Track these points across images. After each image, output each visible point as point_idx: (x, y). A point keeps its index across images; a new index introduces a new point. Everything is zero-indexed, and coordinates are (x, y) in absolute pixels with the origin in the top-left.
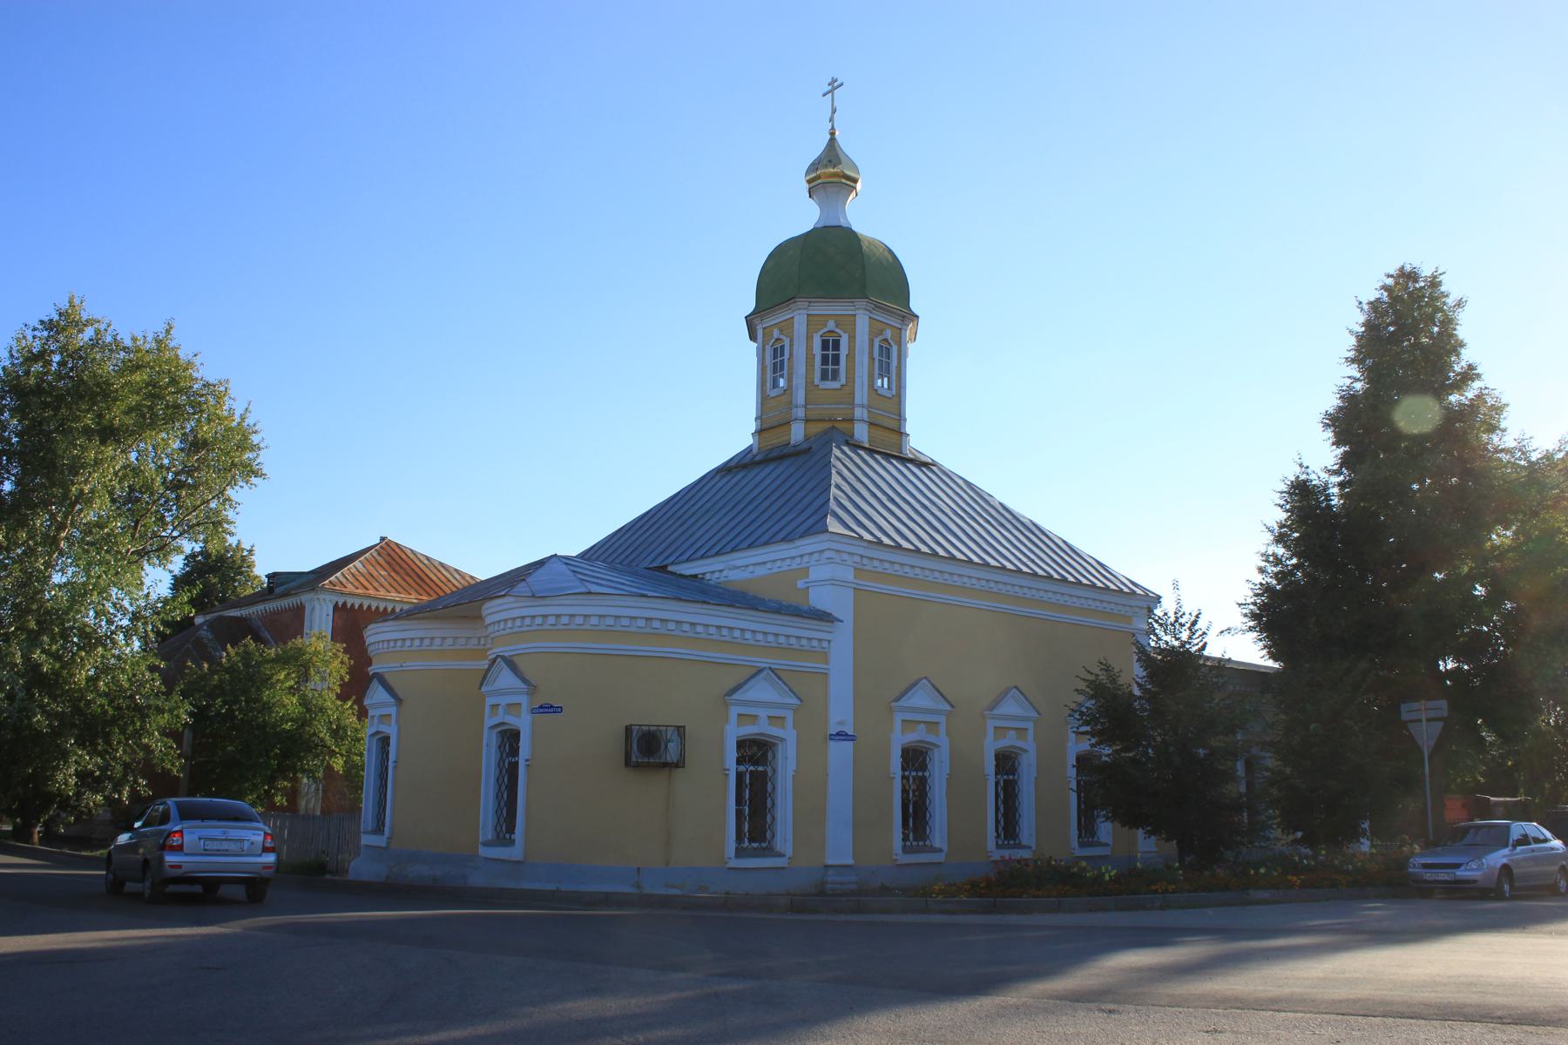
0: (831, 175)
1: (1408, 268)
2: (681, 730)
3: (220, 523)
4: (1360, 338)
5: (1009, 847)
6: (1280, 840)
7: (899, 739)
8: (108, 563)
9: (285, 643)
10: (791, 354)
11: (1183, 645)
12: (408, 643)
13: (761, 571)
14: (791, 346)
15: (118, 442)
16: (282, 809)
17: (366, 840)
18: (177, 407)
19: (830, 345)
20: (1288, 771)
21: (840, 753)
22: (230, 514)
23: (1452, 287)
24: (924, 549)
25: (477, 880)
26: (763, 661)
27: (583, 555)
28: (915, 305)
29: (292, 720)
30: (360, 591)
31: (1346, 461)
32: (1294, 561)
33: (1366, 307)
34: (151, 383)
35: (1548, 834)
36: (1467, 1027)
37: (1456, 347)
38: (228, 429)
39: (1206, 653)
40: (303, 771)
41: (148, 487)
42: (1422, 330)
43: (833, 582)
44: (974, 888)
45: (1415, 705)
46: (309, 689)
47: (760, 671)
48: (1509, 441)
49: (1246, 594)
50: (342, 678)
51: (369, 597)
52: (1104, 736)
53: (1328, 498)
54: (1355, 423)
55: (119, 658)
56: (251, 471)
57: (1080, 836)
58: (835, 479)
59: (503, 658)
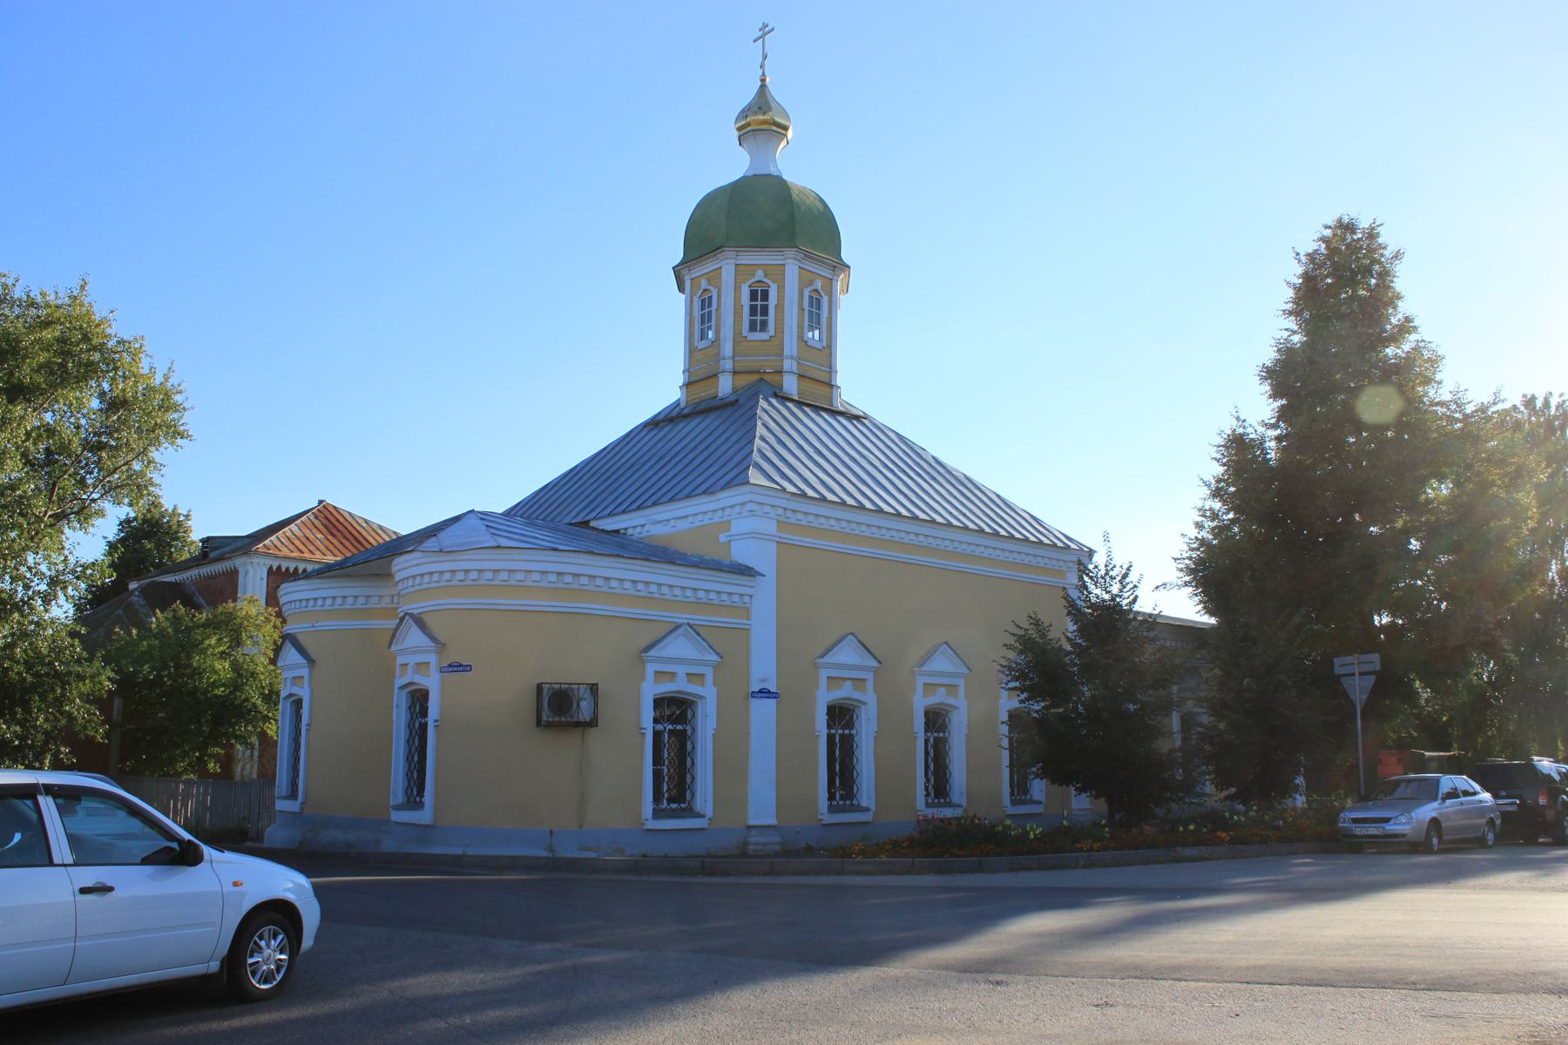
0: (761, 122)
1: (1346, 220)
2: (594, 688)
4: (1297, 289)
5: (939, 805)
6: (1211, 794)
7: (824, 697)
8: (21, 526)
11: (1113, 599)
13: (683, 525)
14: (719, 296)
15: (29, 401)
16: (214, 776)
17: (281, 805)
18: (90, 364)
19: (759, 295)
20: (1222, 726)
21: (763, 714)
23: (1390, 239)
24: (850, 501)
25: (389, 845)
26: (680, 617)
27: (509, 513)
28: (845, 256)
29: (224, 685)
31: (1283, 414)
32: (1231, 516)
33: (1304, 259)
34: (62, 340)
35: (1477, 787)
36: (1378, 994)
38: (149, 388)
39: (1136, 608)
40: (237, 738)
41: (64, 448)
42: (1360, 282)
43: (755, 535)
44: (896, 847)
45: (1349, 659)
46: (238, 654)
47: (678, 627)
48: (1445, 395)
49: (1180, 548)
52: (1033, 692)
53: (1264, 452)
54: (1289, 377)
55: (38, 624)
56: (175, 433)
57: (1012, 794)
58: (760, 430)
59: (411, 615)
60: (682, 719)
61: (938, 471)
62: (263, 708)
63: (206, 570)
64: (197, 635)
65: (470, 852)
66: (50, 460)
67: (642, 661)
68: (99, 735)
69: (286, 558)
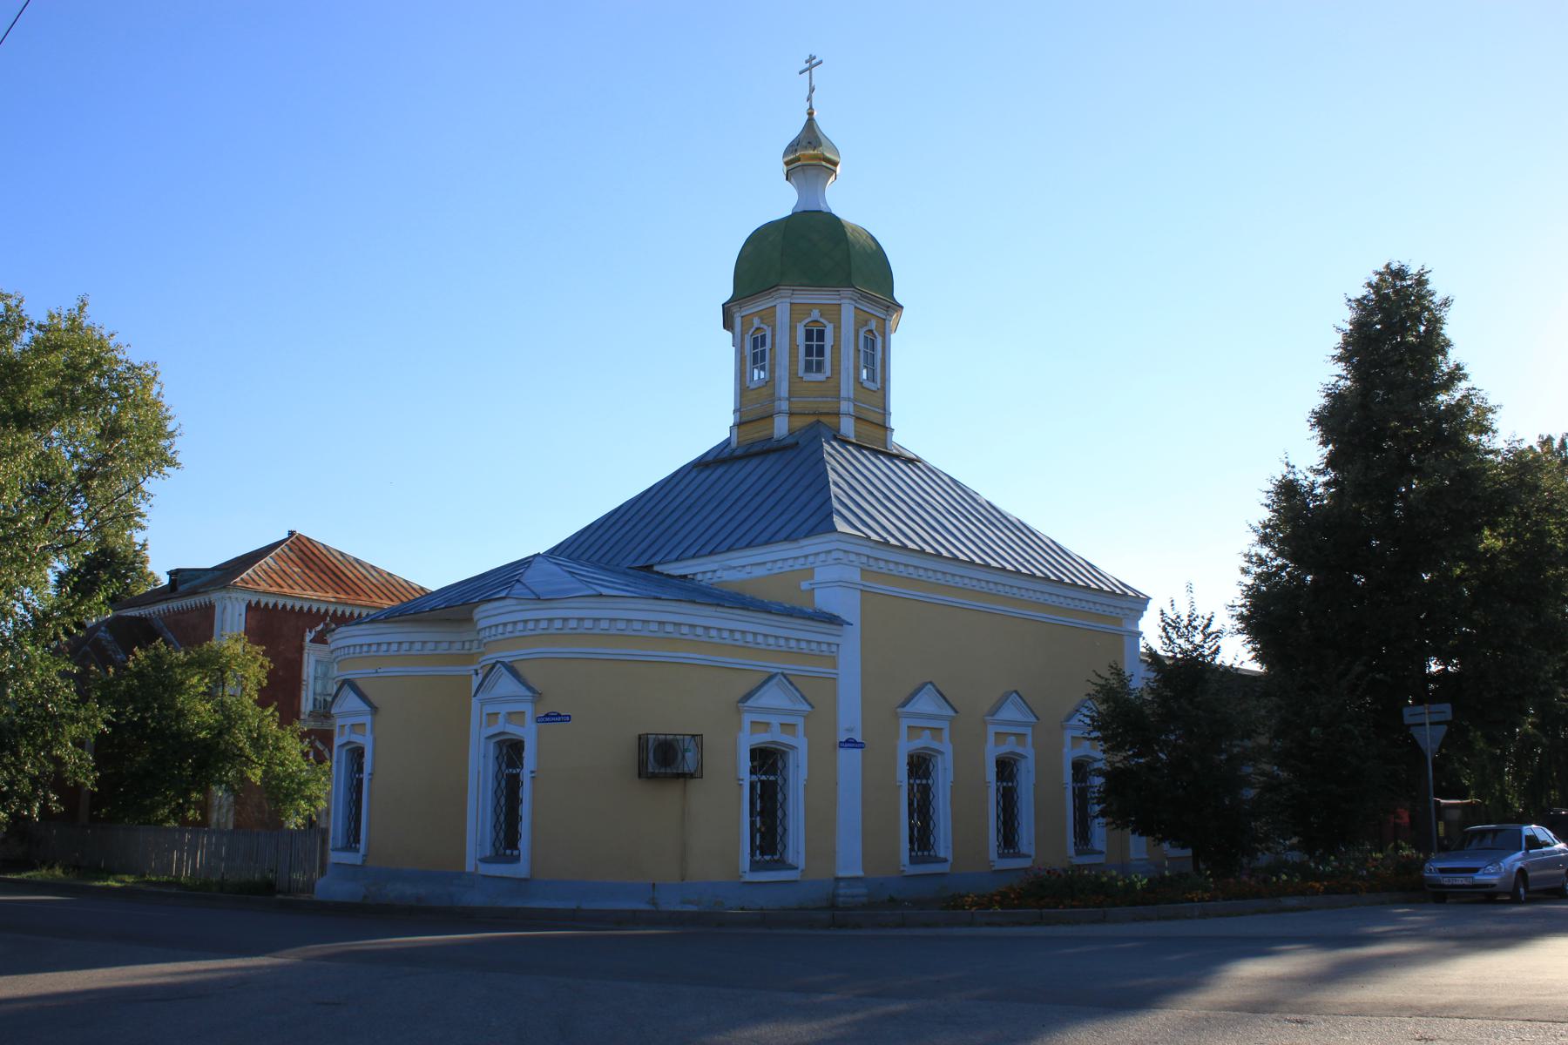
0: (809, 157)
1: (1395, 266)
3: (130, 516)
6: (1289, 850)
7: (905, 747)
9: (201, 645)
10: (773, 344)
12: (384, 647)
13: (759, 572)
14: (773, 336)
16: (195, 823)
19: (815, 335)
22: (143, 508)
23: (1439, 287)
25: (475, 899)
26: (774, 666)
28: (898, 295)
30: (275, 589)
31: (1332, 462)
32: (1279, 562)
34: (72, 365)
37: (1444, 347)
42: (1408, 329)
44: (985, 902)
47: (771, 677)
50: (259, 683)
51: (284, 595)
52: (1113, 742)
58: (832, 476)
59: (503, 663)
60: (773, 769)
61: (994, 517)
62: (248, 750)
63: (175, 605)
64: (178, 674)
65: (585, 906)
66: (44, 491)
67: (739, 712)
68: (89, 781)
69: (265, 593)
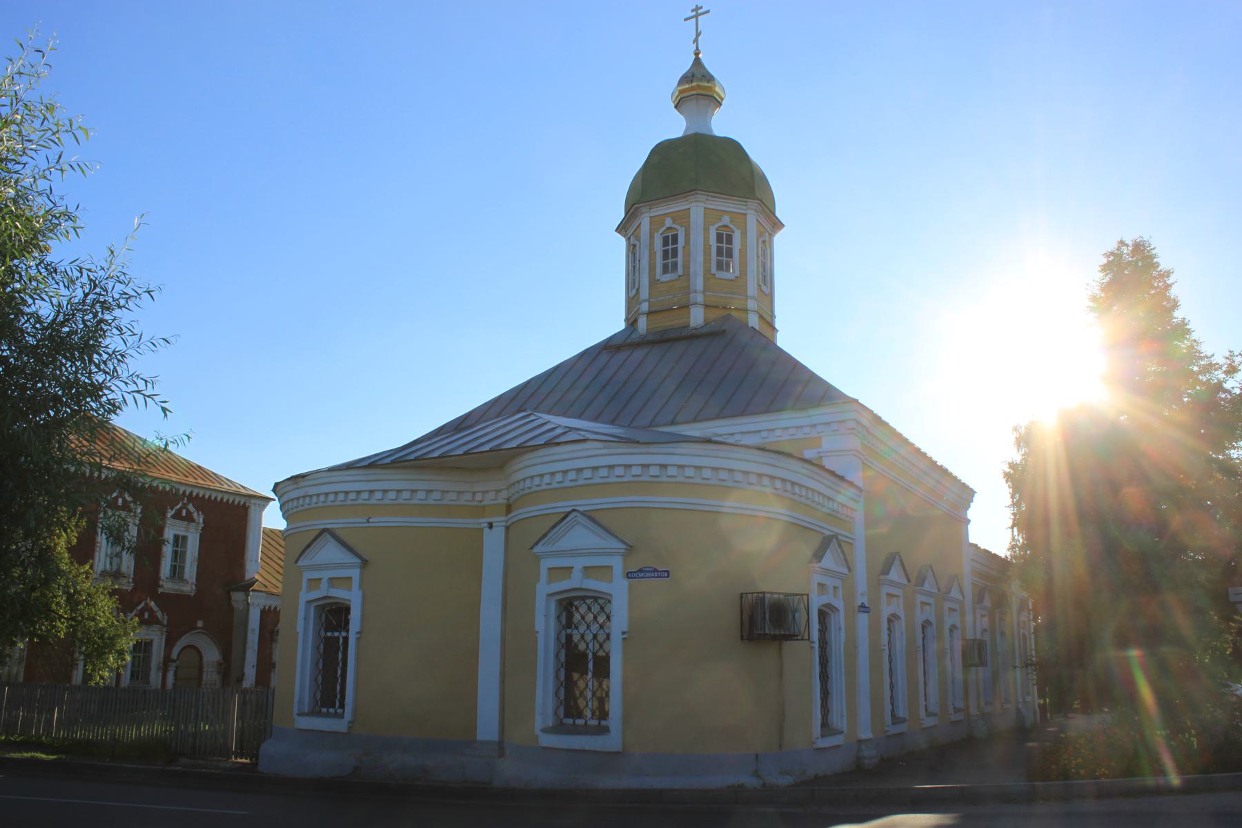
0: (697, 89)
10: (687, 242)
12: (341, 497)
14: (687, 235)
19: (670, 240)
26: (563, 506)
